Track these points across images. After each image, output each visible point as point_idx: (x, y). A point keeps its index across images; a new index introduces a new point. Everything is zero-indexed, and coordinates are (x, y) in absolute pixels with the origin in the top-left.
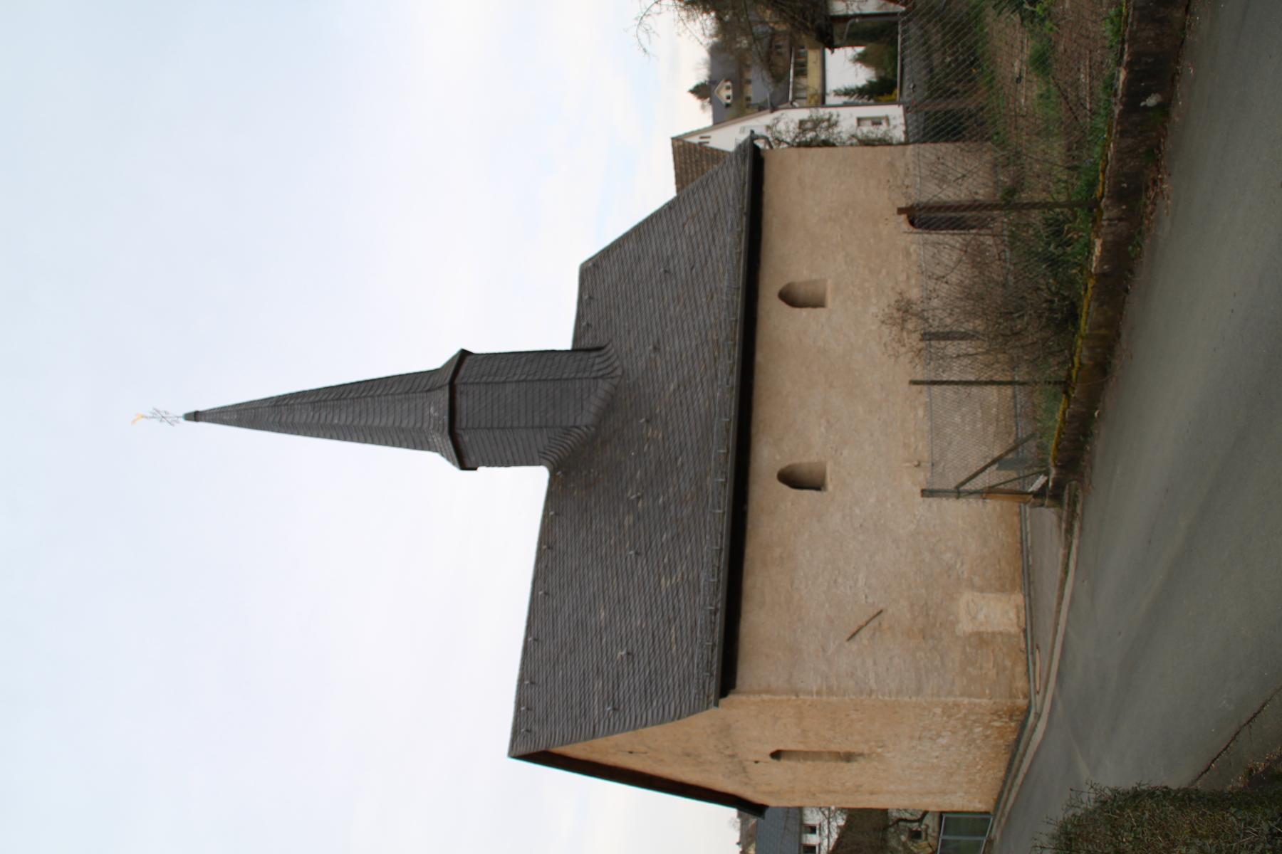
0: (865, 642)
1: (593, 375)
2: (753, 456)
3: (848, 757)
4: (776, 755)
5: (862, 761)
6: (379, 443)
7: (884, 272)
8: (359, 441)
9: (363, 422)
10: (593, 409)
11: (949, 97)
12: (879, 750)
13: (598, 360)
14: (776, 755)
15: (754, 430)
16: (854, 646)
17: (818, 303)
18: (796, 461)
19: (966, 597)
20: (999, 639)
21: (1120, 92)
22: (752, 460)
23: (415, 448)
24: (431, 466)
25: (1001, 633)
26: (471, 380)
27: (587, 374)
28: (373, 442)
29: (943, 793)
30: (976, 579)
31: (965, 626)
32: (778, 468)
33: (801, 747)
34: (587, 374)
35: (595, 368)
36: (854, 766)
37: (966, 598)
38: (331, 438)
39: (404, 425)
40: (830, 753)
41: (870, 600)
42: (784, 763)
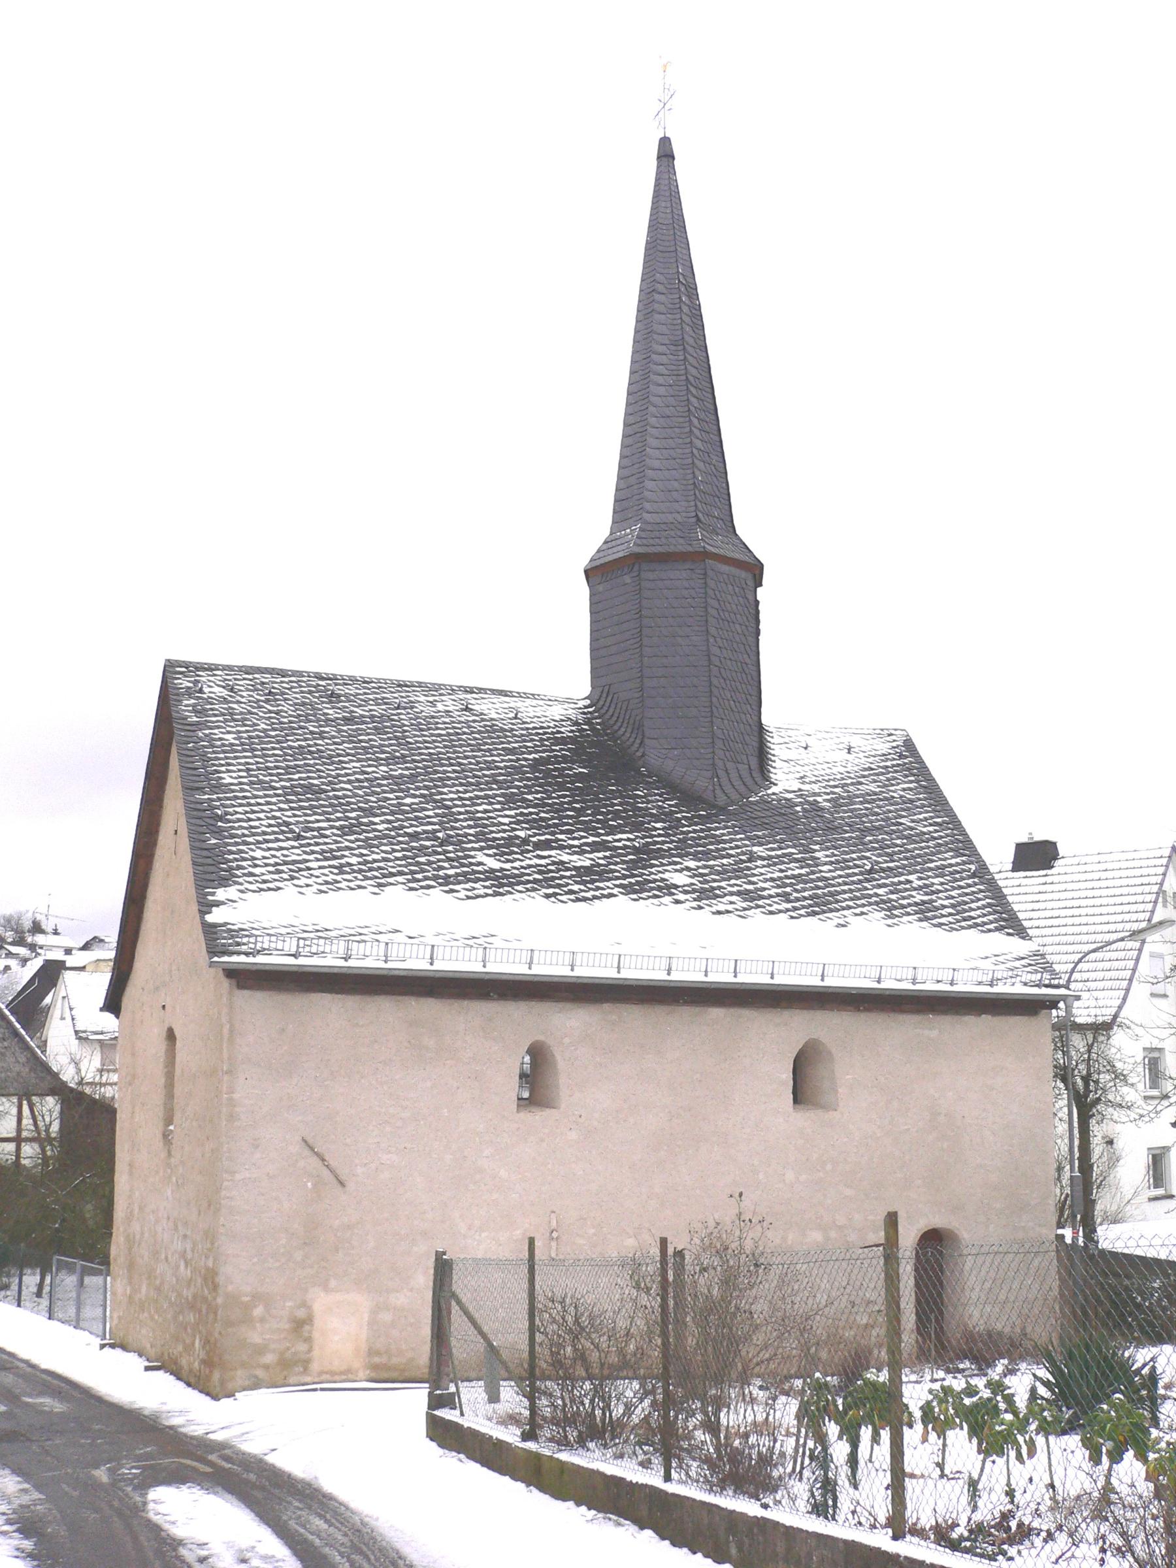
0: (301, 1164)
1: (720, 764)
2: (568, 1005)
3: (166, 1136)
4: (171, 1036)
5: (163, 1155)
6: (624, 446)
7: (849, 1192)
8: (628, 414)
9: (653, 421)
10: (670, 764)
11: (941, 1284)
12: (174, 1179)
13: (743, 768)
14: (171, 1036)
15: (606, 1006)
16: (296, 1148)
17: (800, 1095)
18: (561, 1064)
19: (363, 1302)
20: (302, 1347)
21: (564, 1456)
22: (561, 1005)
23: (617, 501)
24: (590, 525)
25: (310, 1350)
26: (711, 584)
27: (720, 753)
28: (625, 436)
29: (131, 1266)
30: (386, 1317)
31: (320, 1301)
32: (550, 1042)
33: (178, 1072)
34: (720, 753)
35: (730, 765)
36: (159, 1143)
37: (363, 1302)
38: (632, 372)
39: (649, 484)
40: (172, 1110)
41: (359, 1170)
42: (160, 1047)
